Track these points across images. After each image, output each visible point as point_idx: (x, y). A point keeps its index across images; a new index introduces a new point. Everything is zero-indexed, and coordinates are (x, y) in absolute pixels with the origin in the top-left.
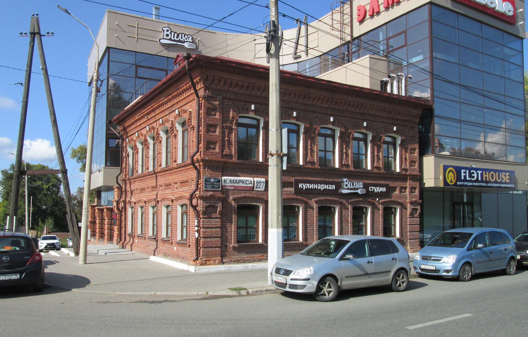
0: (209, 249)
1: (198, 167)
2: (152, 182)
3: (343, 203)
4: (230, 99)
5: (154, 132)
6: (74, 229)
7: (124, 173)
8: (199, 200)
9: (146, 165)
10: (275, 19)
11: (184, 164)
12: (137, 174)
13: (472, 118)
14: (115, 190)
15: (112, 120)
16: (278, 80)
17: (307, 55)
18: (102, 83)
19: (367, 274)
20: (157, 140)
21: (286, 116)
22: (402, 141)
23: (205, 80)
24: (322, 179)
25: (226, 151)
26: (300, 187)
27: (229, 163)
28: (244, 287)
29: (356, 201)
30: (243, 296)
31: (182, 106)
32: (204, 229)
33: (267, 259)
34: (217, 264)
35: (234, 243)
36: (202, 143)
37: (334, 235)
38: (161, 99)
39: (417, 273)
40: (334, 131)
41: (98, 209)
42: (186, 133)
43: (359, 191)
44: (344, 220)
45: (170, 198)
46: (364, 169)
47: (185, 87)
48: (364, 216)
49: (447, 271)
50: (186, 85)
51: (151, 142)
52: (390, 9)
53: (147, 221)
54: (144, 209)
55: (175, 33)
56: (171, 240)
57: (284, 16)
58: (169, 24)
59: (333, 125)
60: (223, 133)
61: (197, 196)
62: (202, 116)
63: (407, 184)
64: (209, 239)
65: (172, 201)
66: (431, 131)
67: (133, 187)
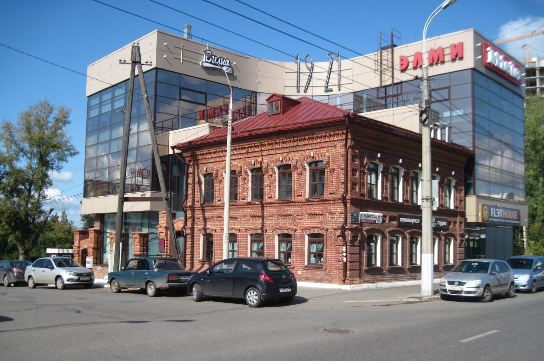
17: (340, 90)
49: (524, 286)
55: (215, 56)
60: (360, 176)
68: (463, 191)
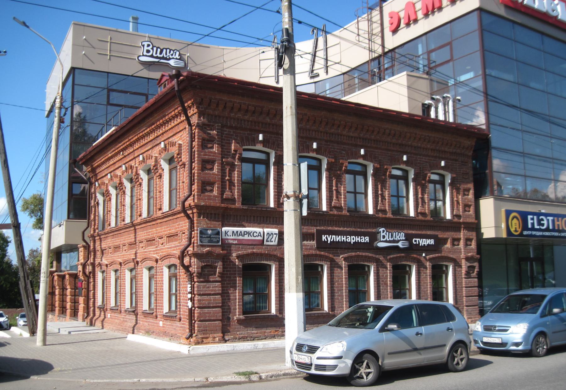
0: (207, 323)
1: (191, 215)
2: (130, 237)
3: (379, 259)
4: (231, 127)
5: (132, 172)
6: (28, 301)
7: (93, 227)
8: (193, 258)
9: (121, 215)
10: (289, 27)
11: (172, 211)
12: (110, 227)
13: (538, 151)
14: (80, 249)
15: (78, 159)
16: (294, 102)
18: (66, 111)
19: (416, 349)
20: (136, 183)
21: (303, 149)
22: (453, 179)
23: (199, 104)
24: (352, 229)
25: (227, 194)
26: (323, 240)
27: (231, 209)
28: (255, 371)
29: (397, 257)
30: (254, 382)
31: (169, 138)
32: (199, 297)
33: (283, 335)
34: (217, 342)
35: (239, 315)
36: (196, 184)
37: (369, 300)
38: (142, 130)
39: (478, 348)
40: (365, 166)
41: (58, 275)
42: (174, 172)
43: (400, 245)
44: (381, 282)
45: (154, 257)
46: (405, 216)
47: (173, 113)
48: (407, 276)
49: (517, 344)
50: (174, 110)
51: (127, 185)
52: (431, 16)
53: (123, 289)
54: (118, 273)
55: (157, 48)
56: (155, 313)
57: (300, 22)
58: (150, 37)
59: (364, 160)
60: (223, 171)
61: (190, 253)
62: (195, 149)
63: (460, 235)
64: (206, 310)
65: (157, 261)
66: (488, 168)
67: (103, 245)
68: (472, 192)
